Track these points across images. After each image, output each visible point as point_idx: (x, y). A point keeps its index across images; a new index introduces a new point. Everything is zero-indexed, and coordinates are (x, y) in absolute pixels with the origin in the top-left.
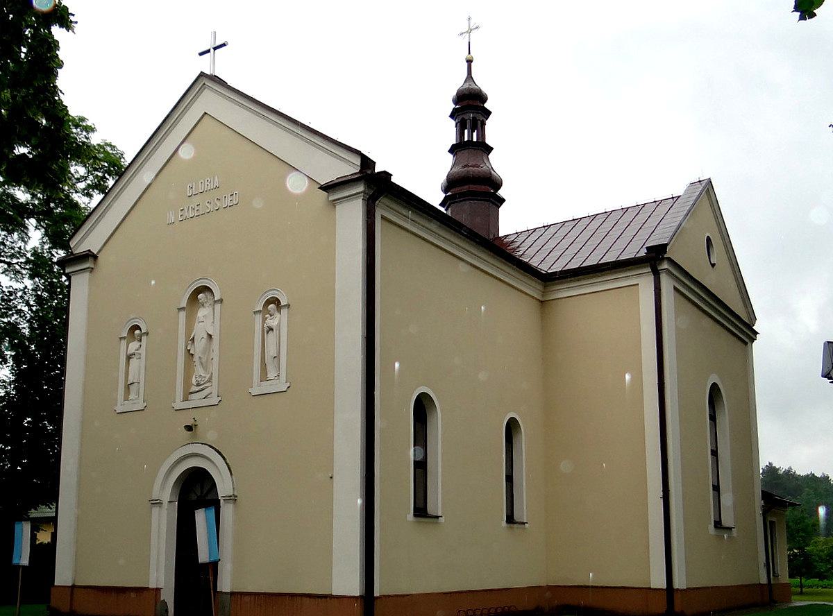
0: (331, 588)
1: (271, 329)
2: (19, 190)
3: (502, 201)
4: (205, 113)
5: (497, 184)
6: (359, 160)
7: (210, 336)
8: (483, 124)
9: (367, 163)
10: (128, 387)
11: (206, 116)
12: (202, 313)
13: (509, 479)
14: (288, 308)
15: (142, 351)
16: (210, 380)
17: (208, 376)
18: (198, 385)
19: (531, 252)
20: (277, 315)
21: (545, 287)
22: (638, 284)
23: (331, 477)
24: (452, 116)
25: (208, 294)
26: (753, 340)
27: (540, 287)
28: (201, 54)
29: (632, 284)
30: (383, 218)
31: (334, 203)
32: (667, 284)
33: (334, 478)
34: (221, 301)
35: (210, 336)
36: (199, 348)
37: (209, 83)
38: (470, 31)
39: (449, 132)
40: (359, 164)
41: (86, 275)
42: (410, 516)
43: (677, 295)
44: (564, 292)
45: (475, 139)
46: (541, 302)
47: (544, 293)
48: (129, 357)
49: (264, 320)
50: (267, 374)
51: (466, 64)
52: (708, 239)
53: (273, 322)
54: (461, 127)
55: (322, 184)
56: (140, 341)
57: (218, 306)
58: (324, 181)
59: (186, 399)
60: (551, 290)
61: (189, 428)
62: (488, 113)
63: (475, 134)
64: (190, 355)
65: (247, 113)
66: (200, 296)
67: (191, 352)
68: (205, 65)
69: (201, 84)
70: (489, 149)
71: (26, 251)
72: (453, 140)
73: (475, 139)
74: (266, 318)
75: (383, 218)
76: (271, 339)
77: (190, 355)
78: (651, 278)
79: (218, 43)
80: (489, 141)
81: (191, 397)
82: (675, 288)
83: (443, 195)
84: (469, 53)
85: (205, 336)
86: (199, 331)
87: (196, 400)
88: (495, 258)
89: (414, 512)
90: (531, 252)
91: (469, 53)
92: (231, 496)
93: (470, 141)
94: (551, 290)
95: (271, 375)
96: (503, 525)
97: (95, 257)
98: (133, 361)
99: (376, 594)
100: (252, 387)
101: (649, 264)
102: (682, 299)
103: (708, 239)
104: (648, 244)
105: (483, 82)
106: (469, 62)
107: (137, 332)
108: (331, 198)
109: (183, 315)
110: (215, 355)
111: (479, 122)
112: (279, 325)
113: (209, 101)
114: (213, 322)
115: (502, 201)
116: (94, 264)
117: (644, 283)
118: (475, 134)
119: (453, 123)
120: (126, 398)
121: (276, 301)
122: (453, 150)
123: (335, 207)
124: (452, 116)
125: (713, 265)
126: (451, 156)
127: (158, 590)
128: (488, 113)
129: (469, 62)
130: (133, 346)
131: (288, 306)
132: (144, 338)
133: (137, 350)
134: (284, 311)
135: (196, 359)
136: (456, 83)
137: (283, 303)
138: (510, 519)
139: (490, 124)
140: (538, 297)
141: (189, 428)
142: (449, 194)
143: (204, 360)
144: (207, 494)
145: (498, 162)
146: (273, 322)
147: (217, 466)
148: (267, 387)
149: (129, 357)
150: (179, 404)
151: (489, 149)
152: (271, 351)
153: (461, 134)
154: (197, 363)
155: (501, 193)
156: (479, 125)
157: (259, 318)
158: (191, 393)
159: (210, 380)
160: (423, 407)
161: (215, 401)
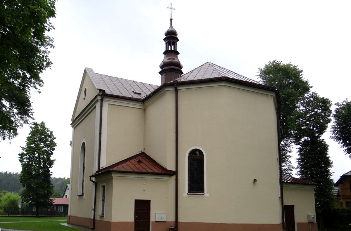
2: (289, 152)
22: (140, 94)
24: (165, 40)
39: (163, 47)
51: (170, 21)
52: (84, 144)
70: (178, 53)
71: (11, 61)
72: (164, 50)
80: (177, 50)
83: (165, 37)
84: (171, 17)
88: (248, 88)
91: (171, 17)
93: (171, 50)
103: (84, 144)
105: (176, 27)
106: (171, 20)
114: (84, 99)
122: (164, 53)
126: (163, 56)
127: (183, 73)
129: (171, 20)
139: (178, 43)
142: (164, 69)
151: (178, 53)
153: (167, 47)
156: (174, 44)
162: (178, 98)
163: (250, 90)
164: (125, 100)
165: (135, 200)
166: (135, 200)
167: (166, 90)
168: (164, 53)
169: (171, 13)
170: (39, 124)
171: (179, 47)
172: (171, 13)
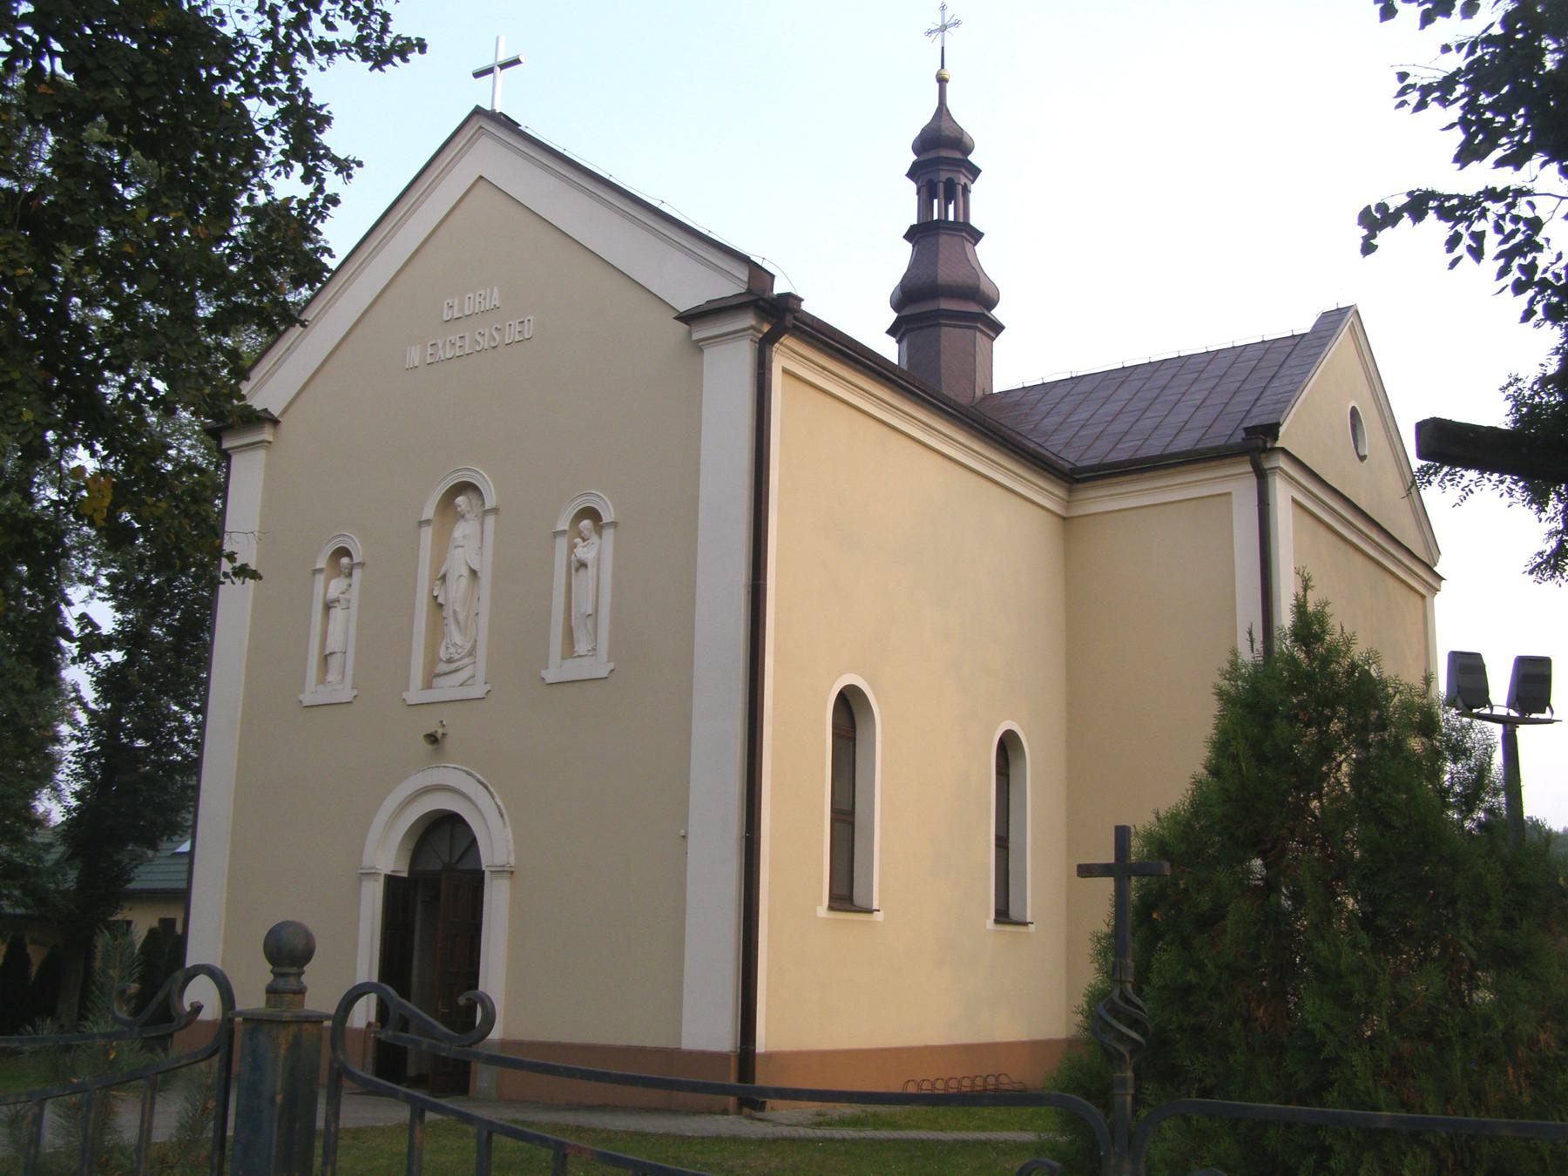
0: (680, 1043)
1: (583, 565)
3: (997, 328)
4: (481, 177)
5: (991, 302)
6: (747, 273)
7: (474, 573)
8: (966, 190)
9: (759, 276)
10: (325, 659)
11: (482, 184)
12: (462, 530)
13: (1002, 842)
14: (616, 527)
15: (354, 595)
16: (472, 652)
17: (468, 646)
18: (450, 661)
19: (1052, 420)
20: (594, 538)
21: (1070, 491)
22: (1230, 493)
23: (684, 837)
24: (912, 174)
25: (472, 496)
26: (1435, 591)
27: (1059, 492)
28: (477, 75)
29: (1210, 493)
30: (785, 371)
31: (698, 347)
32: (1282, 494)
33: (690, 837)
34: (495, 510)
35: (474, 573)
36: (457, 588)
37: (490, 127)
38: (943, 28)
39: (905, 205)
40: (746, 279)
41: (260, 456)
42: (822, 910)
43: (1298, 511)
44: (1102, 501)
45: (951, 218)
46: (1064, 519)
47: (1068, 503)
48: (328, 607)
49: (573, 547)
50: (573, 647)
51: (937, 85)
52: (1354, 412)
53: (584, 552)
54: (927, 193)
55: (681, 311)
56: (350, 575)
57: (490, 521)
58: (683, 307)
59: (428, 685)
60: (1081, 497)
61: (433, 739)
62: (975, 172)
63: (951, 207)
64: (438, 606)
65: (552, 182)
66: (461, 500)
67: (441, 600)
68: (482, 94)
69: (476, 128)
70: (977, 236)
73: (951, 218)
74: (575, 546)
75: (785, 371)
76: (585, 581)
77: (438, 606)
78: (1251, 483)
79: (502, 58)
80: (975, 221)
81: (438, 682)
82: (1294, 501)
83: (893, 316)
84: (943, 67)
85: (465, 572)
86: (457, 564)
87: (447, 689)
89: (996, 916)
90: (1052, 420)
92: (503, 866)
94: (1081, 497)
95: (582, 647)
96: (988, 927)
97: (275, 422)
98: (337, 614)
99: (761, 1047)
100: (547, 668)
101: (1248, 458)
102: (1307, 520)
103: (1354, 412)
104: (1247, 424)
105: (964, 116)
106: (942, 81)
107: (345, 560)
108: (696, 336)
109: (427, 534)
110: (485, 607)
111: (960, 188)
112: (598, 558)
113: (488, 158)
115: (997, 328)
116: (274, 435)
117: (1238, 485)
118: (951, 207)
119: (912, 187)
120: (322, 679)
121: (591, 514)
123: (702, 351)
124: (912, 174)
125: (1362, 458)
128: (975, 172)
129: (942, 81)
130: (336, 587)
131: (614, 524)
132: (357, 573)
133: (343, 593)
134: (609, 534)
135: (448, 612)
136: (923, 116)
137: (606, 519)
138: (1003, 916)
139: (977, 189)
140: (1060, 512)
141: (433, 739)
143: (461, 617)
144: (458, 862)
145: (991, 259)
146: (584, 552)
147: (479, 811)
148: (573, 670)
149: (328, 607)
150: (415, 694)
151: (977, 236)
152: (583, 604)
153: (925, 206)
154: (451, 621)
155: (997, 313)
156: (955, 192)
157: (562, 544)
158: (439, 675)
159: (472, 652)
160: (850, 707)
161: (479, 690)
162: (1271, 506)
163: (1139, 488)
164: (997, 446)
165: (904, 237)
166: (904, 237)
167: (979, 325)
168: (911, 235)
169: (943, 48)
170: (228, 46)
171: (983, 204)
172: (943, 48)
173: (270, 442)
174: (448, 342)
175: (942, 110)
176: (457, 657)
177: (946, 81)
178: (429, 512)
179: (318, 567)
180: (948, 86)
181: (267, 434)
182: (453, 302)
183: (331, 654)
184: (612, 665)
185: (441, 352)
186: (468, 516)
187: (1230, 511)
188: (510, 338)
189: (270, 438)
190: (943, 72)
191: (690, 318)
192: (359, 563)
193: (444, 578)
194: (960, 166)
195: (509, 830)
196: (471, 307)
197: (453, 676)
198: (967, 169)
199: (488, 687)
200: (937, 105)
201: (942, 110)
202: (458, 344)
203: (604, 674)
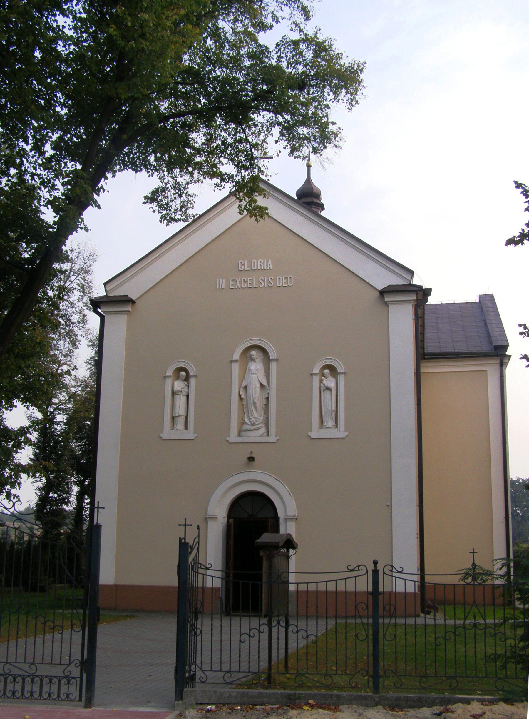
1: (329, 389)
10: (173, 418)
18: (253, 424)
51: (307, 168)
59: (239, 435)
66: (253, 353)
85: (258, 385)
97: (133, 302)
105: (316, 182)
109: (236, 368)
121: (332, 369)
150: (233, 437)
173: (129, 312)
174: (242, 281)
175: (308, 180)
176: (257, 423)
177: (310, 166)
178: (236, 356)
179: (168, 374)
180: (312, 169)
181: (129, 308)
182: (245, 262)
183: (179, 416)
184: (347, 433)
185: (238, 284)
186: (256, 360)
187: (487, 374)
188: (280, 284)
189: (130, 310)
190: (309, 162)
191: (383, 293)
192: (194, 376)
193: (245, 387)
194: (320, 207)
195: (294, 501)
196: (256, 266)
197: (255, 431)
198: (315, 205)
199: (278, 438)
200: (306, 177)
201: (308, 180)
202: (249, 282)
203: (344, 437)
